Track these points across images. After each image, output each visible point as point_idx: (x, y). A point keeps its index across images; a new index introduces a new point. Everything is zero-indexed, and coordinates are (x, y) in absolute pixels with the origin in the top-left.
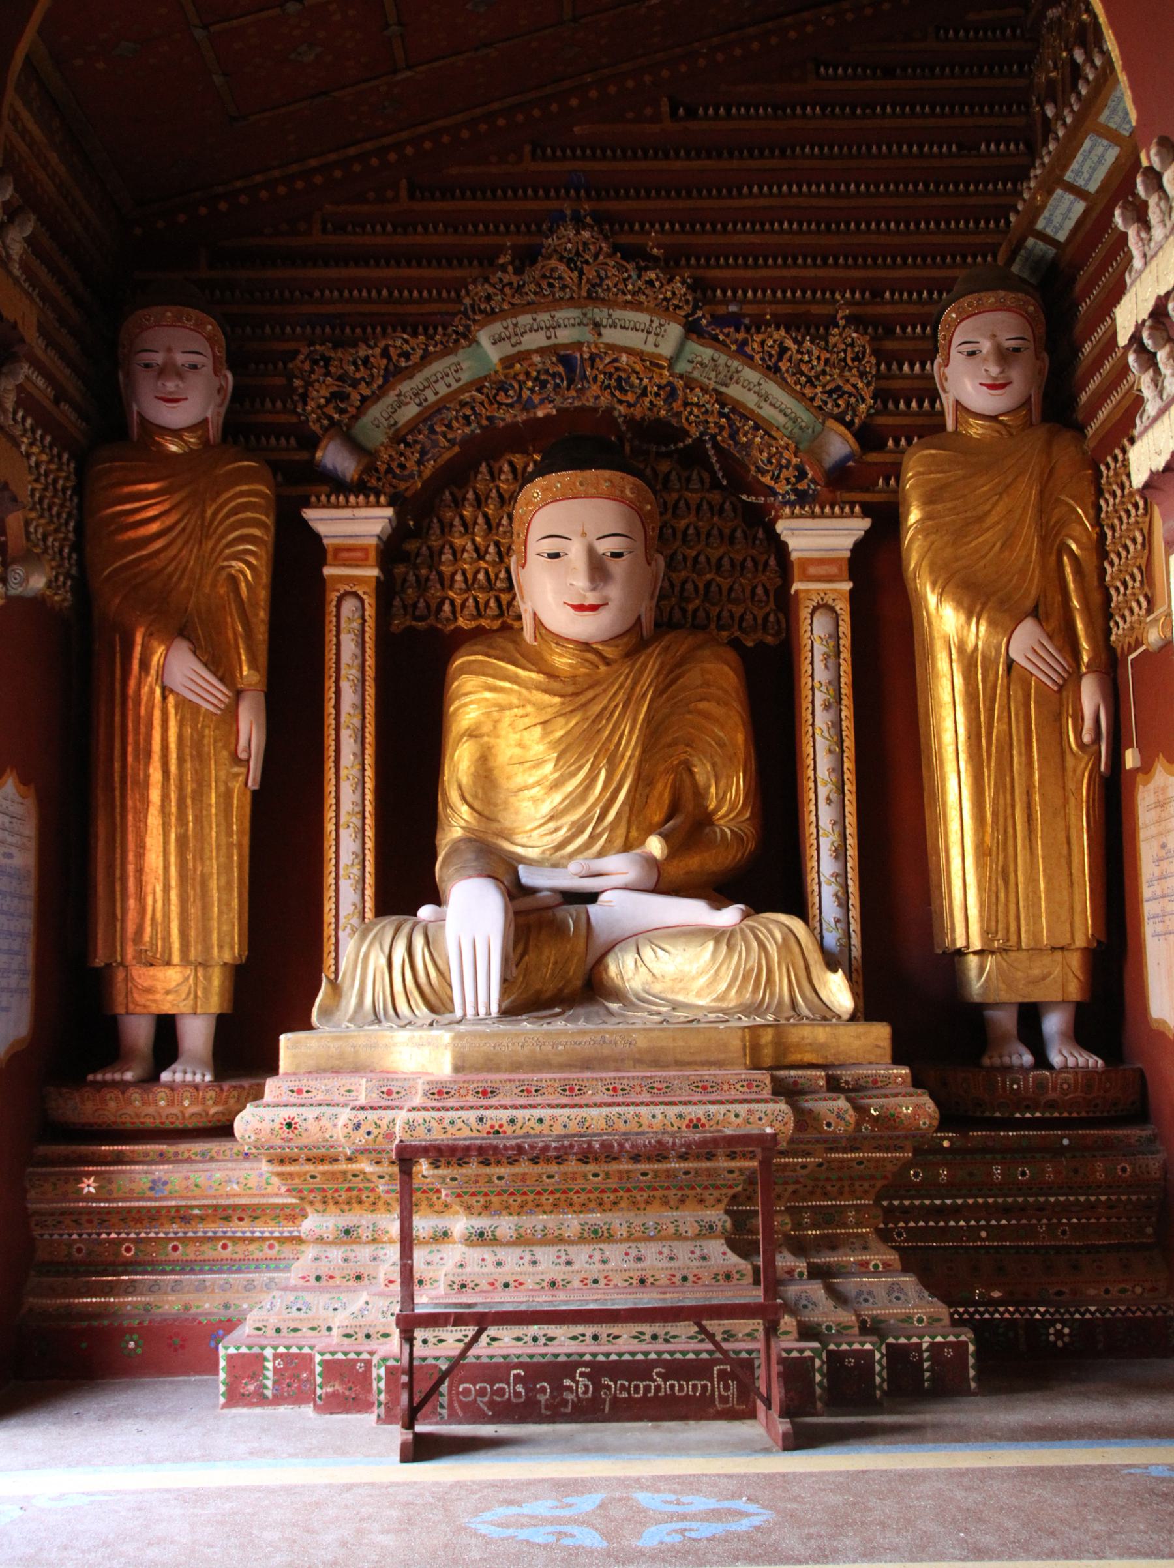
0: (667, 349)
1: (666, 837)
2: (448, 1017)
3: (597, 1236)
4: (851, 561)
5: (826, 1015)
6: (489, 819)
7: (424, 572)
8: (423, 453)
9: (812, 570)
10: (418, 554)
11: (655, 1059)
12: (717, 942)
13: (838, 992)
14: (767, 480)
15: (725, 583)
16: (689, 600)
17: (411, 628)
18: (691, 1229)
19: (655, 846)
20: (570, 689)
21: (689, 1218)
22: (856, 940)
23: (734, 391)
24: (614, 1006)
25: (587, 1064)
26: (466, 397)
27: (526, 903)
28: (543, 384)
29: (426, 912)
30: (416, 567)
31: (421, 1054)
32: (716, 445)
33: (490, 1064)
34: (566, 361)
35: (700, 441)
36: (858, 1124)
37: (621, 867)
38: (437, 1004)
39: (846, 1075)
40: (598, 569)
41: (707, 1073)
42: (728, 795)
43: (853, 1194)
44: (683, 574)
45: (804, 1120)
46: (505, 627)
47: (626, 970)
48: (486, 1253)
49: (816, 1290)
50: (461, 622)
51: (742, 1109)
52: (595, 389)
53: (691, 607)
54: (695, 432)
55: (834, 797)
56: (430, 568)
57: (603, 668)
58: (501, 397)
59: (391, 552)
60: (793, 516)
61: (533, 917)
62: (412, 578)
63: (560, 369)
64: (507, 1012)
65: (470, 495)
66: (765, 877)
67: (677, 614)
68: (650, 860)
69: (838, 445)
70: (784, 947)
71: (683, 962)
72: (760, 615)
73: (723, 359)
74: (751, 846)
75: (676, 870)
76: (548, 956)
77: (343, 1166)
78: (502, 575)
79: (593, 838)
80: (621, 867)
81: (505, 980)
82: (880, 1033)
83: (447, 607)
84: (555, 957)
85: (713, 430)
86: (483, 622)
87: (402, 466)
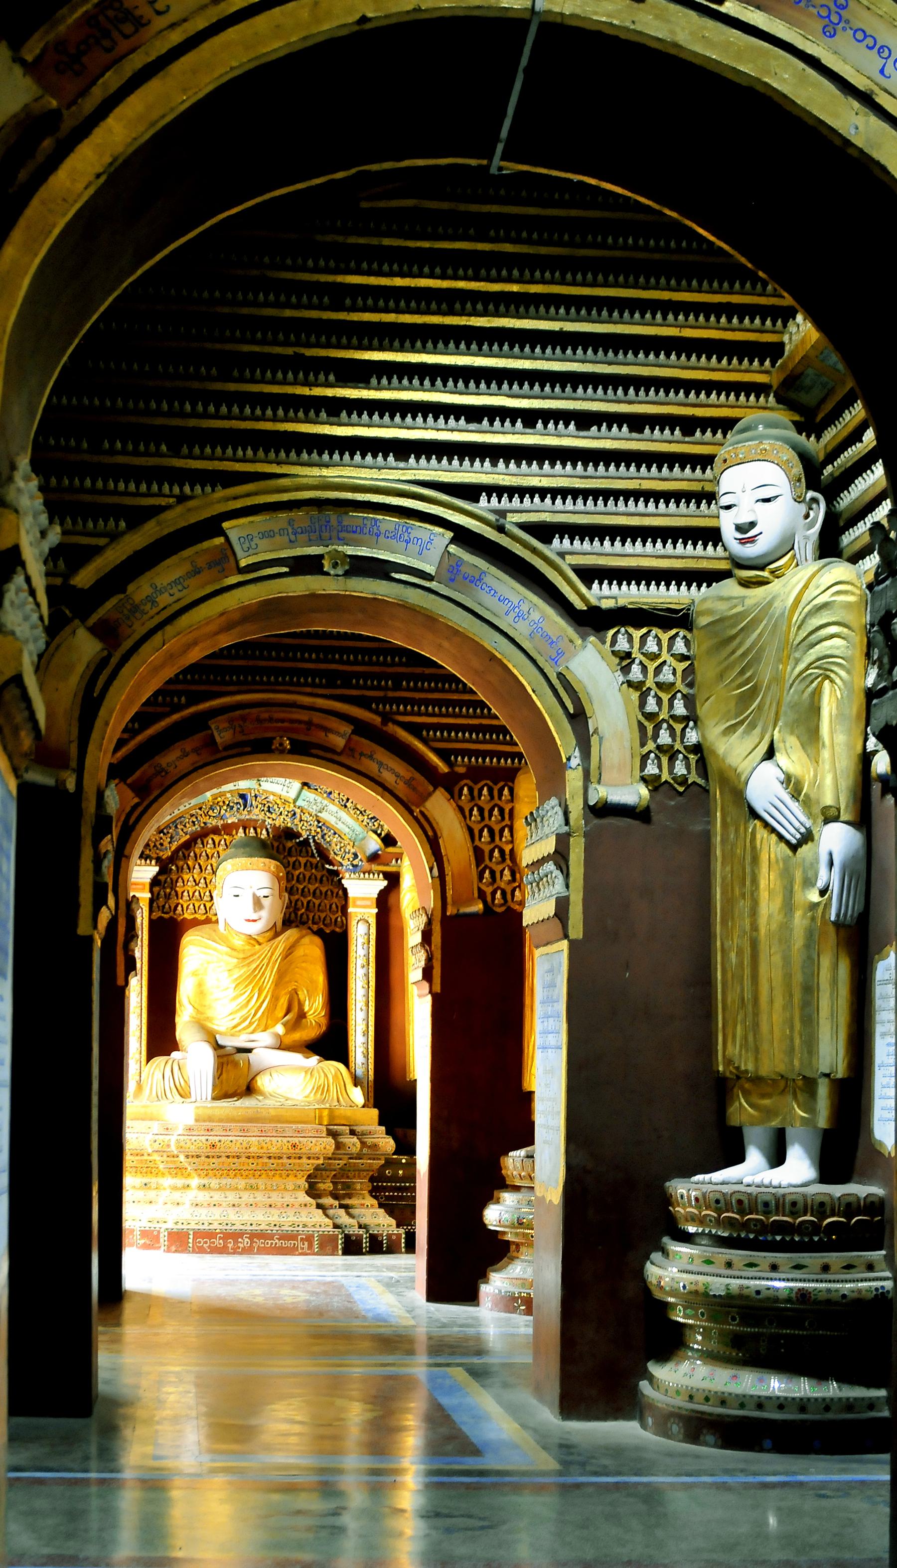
0: (292, 795)
1: (285, 1025)
2: (188, 1100)
3: (252, 1188)
4: (378, 899)
5: (352, 1105)
6: (202, 1013)
7: (168, 890)
8: (171, 838)
9: (359, 903)
10: (165, 882)
11: (278, 1119)
12: (306, 1072)
13: (357, 1095)
14: (338, 858)
15: (317, 902)
16: (299, 910)
17: (161, 917)
18: (291, 1187)
19: (280, 1029)
20: (241, 956)
21: (290, 1183)
22: (371, 1073)
23: (323, 816)
24: (260, 1098)
25: (251, 1120)
26: (193, 812)
27: (221, 1052)
28: (232, 808)
29: (174, 1054)
30: (164, 888)
31: (181, 1115)
32: (314, 841)
33: (210, 1119)
34: (243, 797)
35: (307, 840)
36: (361, 1150)
37: (265, 1038)
38: (184, 1094)
39: (358, 1129)
40: (258, 903)
41: (300, 1126)
42: (315, 1007)
43: (359, 1177)
44: (297, 897)
45: (339, 1145)
46: (208, 921)
47: (262, 1082)
48: (206, 1193)
49: (342, 1212)
50: (186, 916)
51: (314, 1140)
52: (256, 811)
53: (300, 913)
54: (305, 835)
55: (364, 1008)
56: (172, 889)
57: (257, 947)
58: (210, 813)
59: (155, 882)
60: (350, 878)
61: (225, 1059)
62: (162, 893)
63: (241, 801)
64: (213, 1099)
65: (192, 854)
66: (331, 1044)
67: (293, 915)
68: (277, 1036)
69: (374, 844)
70: (335, 1077)
71: (294, 1082)
72: (333, 918)
73: (319, 799)
74: (324, 1028)
75: (288, 1040)
76: (230, 1074)
77: (146, 1157)
78: (207, 894)
79: (251, 1024)
80: (265, 1038)
81: (214, 1086)
82: (375, 1112)
83: (179, 908)
84: (235, 1076)
85: (313, 833)
86: (197, 916)
87: (162, 844)
